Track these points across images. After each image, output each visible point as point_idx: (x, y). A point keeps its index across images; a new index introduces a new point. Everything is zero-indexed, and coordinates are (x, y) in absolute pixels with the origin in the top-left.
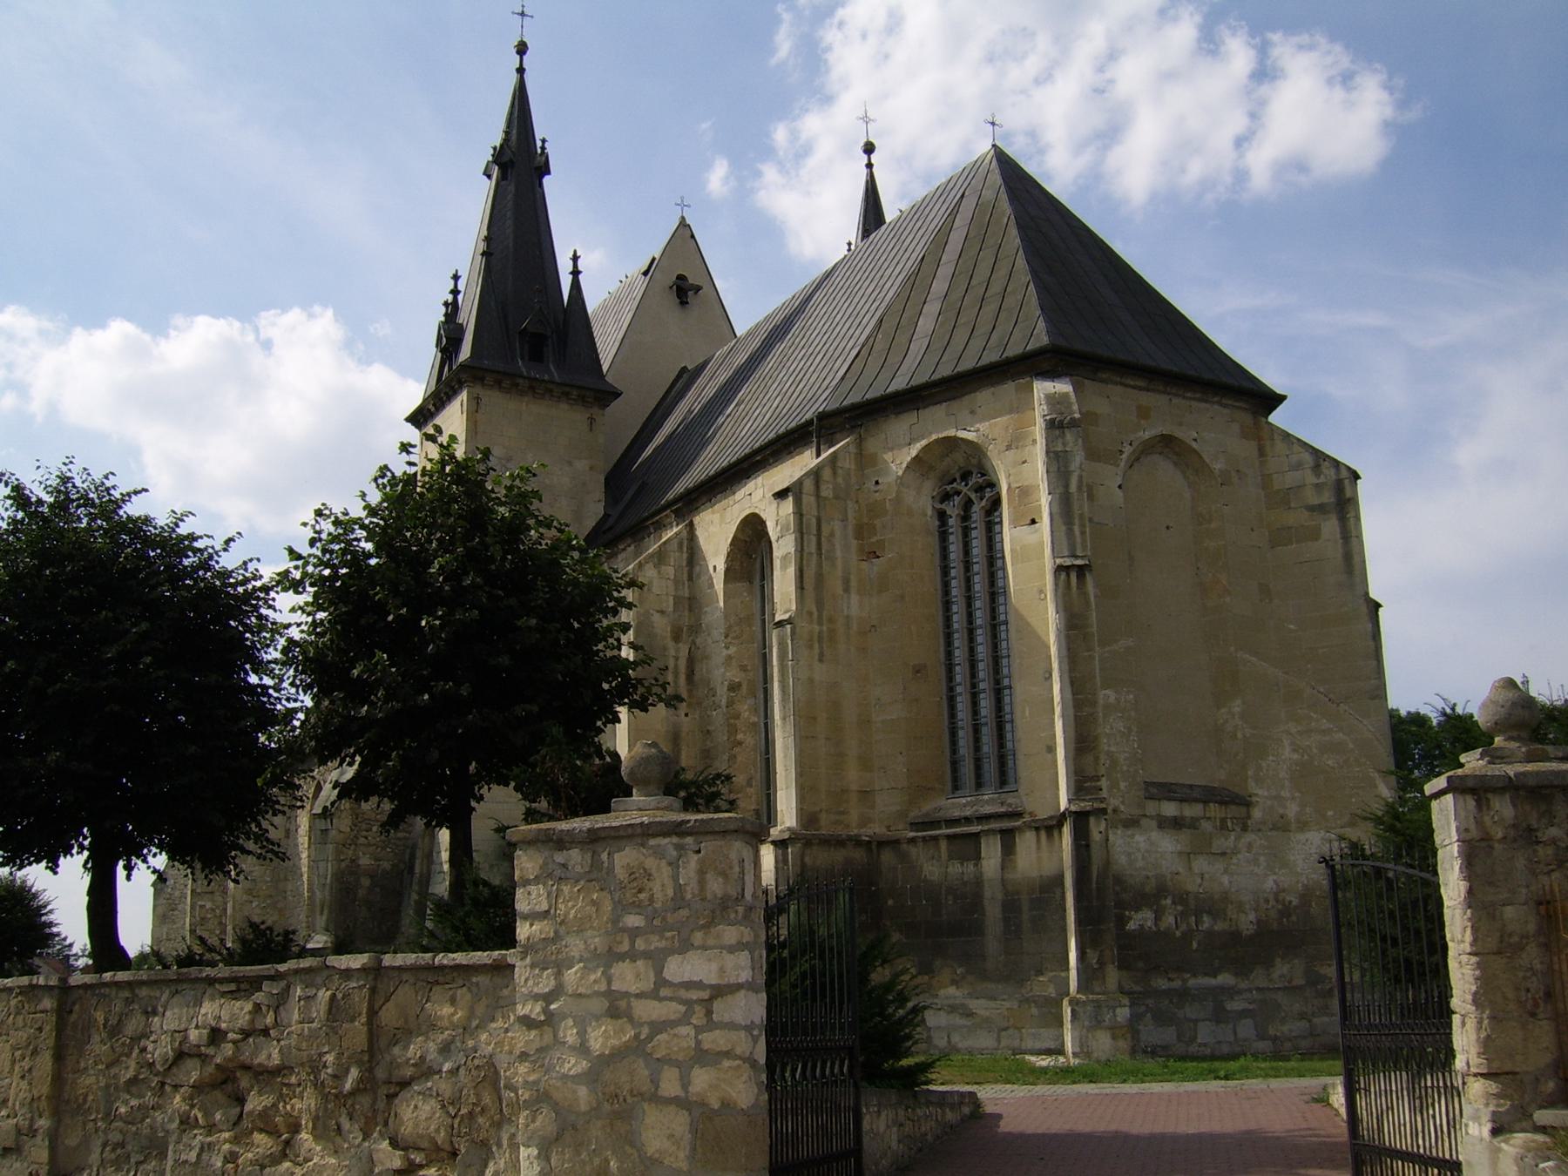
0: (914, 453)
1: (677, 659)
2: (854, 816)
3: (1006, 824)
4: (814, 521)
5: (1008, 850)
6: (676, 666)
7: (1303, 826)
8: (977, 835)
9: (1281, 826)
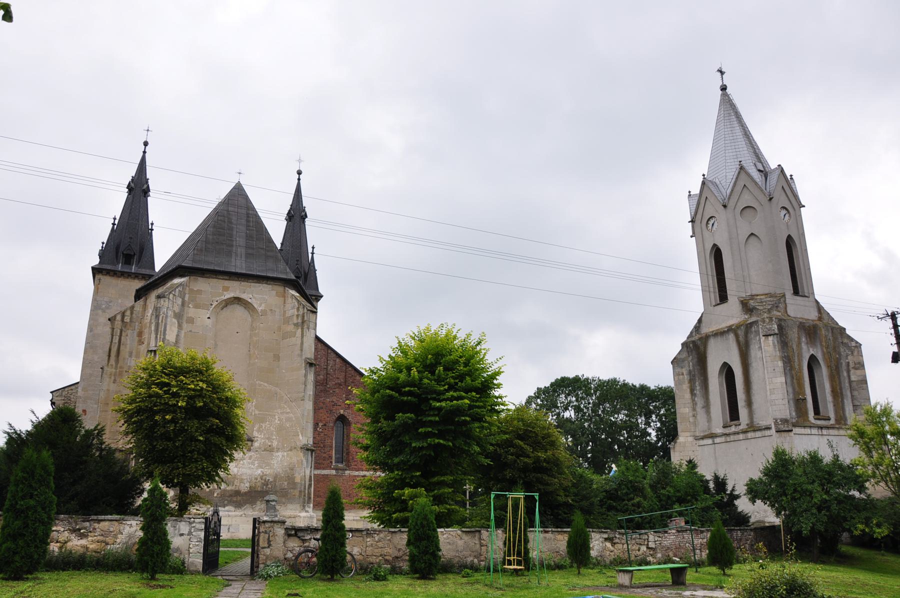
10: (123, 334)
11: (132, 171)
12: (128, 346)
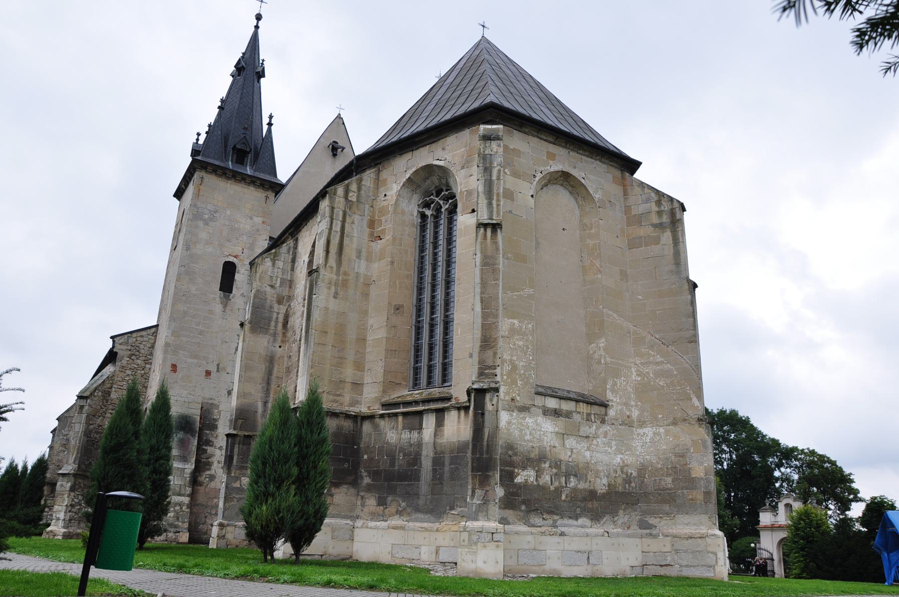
0: (408, 176)
1: (278, 313)
2: (347, 398)
3: (440, 405)
4: (341, 213)
5: (440, 423)
6: (277, 318)
7: (642, 424)
8: (420, 413)
9: (628, 423)
10: (348, 220)
11: (242, 47)
12: (355, 239)
